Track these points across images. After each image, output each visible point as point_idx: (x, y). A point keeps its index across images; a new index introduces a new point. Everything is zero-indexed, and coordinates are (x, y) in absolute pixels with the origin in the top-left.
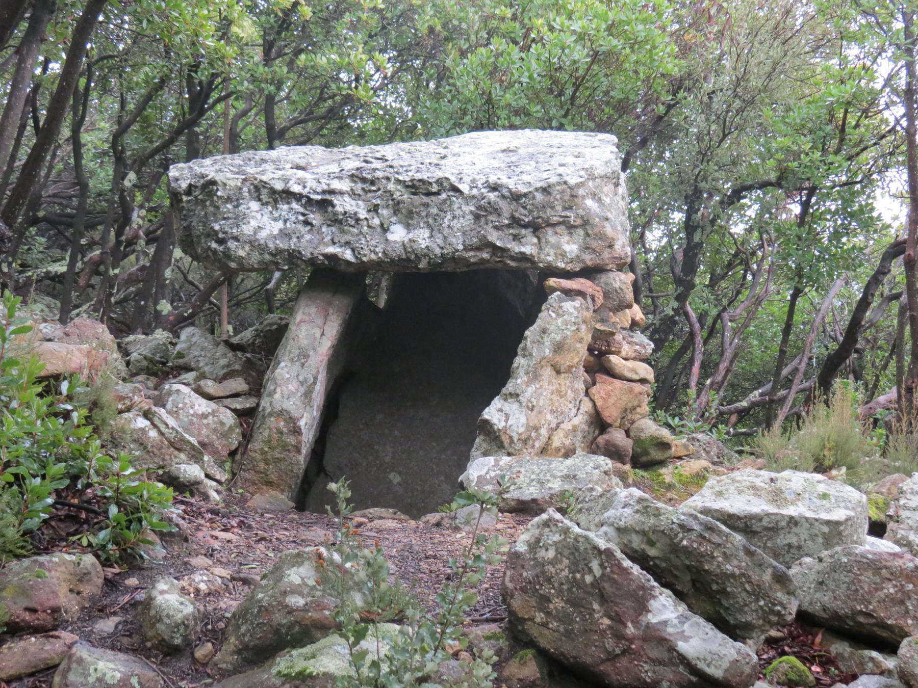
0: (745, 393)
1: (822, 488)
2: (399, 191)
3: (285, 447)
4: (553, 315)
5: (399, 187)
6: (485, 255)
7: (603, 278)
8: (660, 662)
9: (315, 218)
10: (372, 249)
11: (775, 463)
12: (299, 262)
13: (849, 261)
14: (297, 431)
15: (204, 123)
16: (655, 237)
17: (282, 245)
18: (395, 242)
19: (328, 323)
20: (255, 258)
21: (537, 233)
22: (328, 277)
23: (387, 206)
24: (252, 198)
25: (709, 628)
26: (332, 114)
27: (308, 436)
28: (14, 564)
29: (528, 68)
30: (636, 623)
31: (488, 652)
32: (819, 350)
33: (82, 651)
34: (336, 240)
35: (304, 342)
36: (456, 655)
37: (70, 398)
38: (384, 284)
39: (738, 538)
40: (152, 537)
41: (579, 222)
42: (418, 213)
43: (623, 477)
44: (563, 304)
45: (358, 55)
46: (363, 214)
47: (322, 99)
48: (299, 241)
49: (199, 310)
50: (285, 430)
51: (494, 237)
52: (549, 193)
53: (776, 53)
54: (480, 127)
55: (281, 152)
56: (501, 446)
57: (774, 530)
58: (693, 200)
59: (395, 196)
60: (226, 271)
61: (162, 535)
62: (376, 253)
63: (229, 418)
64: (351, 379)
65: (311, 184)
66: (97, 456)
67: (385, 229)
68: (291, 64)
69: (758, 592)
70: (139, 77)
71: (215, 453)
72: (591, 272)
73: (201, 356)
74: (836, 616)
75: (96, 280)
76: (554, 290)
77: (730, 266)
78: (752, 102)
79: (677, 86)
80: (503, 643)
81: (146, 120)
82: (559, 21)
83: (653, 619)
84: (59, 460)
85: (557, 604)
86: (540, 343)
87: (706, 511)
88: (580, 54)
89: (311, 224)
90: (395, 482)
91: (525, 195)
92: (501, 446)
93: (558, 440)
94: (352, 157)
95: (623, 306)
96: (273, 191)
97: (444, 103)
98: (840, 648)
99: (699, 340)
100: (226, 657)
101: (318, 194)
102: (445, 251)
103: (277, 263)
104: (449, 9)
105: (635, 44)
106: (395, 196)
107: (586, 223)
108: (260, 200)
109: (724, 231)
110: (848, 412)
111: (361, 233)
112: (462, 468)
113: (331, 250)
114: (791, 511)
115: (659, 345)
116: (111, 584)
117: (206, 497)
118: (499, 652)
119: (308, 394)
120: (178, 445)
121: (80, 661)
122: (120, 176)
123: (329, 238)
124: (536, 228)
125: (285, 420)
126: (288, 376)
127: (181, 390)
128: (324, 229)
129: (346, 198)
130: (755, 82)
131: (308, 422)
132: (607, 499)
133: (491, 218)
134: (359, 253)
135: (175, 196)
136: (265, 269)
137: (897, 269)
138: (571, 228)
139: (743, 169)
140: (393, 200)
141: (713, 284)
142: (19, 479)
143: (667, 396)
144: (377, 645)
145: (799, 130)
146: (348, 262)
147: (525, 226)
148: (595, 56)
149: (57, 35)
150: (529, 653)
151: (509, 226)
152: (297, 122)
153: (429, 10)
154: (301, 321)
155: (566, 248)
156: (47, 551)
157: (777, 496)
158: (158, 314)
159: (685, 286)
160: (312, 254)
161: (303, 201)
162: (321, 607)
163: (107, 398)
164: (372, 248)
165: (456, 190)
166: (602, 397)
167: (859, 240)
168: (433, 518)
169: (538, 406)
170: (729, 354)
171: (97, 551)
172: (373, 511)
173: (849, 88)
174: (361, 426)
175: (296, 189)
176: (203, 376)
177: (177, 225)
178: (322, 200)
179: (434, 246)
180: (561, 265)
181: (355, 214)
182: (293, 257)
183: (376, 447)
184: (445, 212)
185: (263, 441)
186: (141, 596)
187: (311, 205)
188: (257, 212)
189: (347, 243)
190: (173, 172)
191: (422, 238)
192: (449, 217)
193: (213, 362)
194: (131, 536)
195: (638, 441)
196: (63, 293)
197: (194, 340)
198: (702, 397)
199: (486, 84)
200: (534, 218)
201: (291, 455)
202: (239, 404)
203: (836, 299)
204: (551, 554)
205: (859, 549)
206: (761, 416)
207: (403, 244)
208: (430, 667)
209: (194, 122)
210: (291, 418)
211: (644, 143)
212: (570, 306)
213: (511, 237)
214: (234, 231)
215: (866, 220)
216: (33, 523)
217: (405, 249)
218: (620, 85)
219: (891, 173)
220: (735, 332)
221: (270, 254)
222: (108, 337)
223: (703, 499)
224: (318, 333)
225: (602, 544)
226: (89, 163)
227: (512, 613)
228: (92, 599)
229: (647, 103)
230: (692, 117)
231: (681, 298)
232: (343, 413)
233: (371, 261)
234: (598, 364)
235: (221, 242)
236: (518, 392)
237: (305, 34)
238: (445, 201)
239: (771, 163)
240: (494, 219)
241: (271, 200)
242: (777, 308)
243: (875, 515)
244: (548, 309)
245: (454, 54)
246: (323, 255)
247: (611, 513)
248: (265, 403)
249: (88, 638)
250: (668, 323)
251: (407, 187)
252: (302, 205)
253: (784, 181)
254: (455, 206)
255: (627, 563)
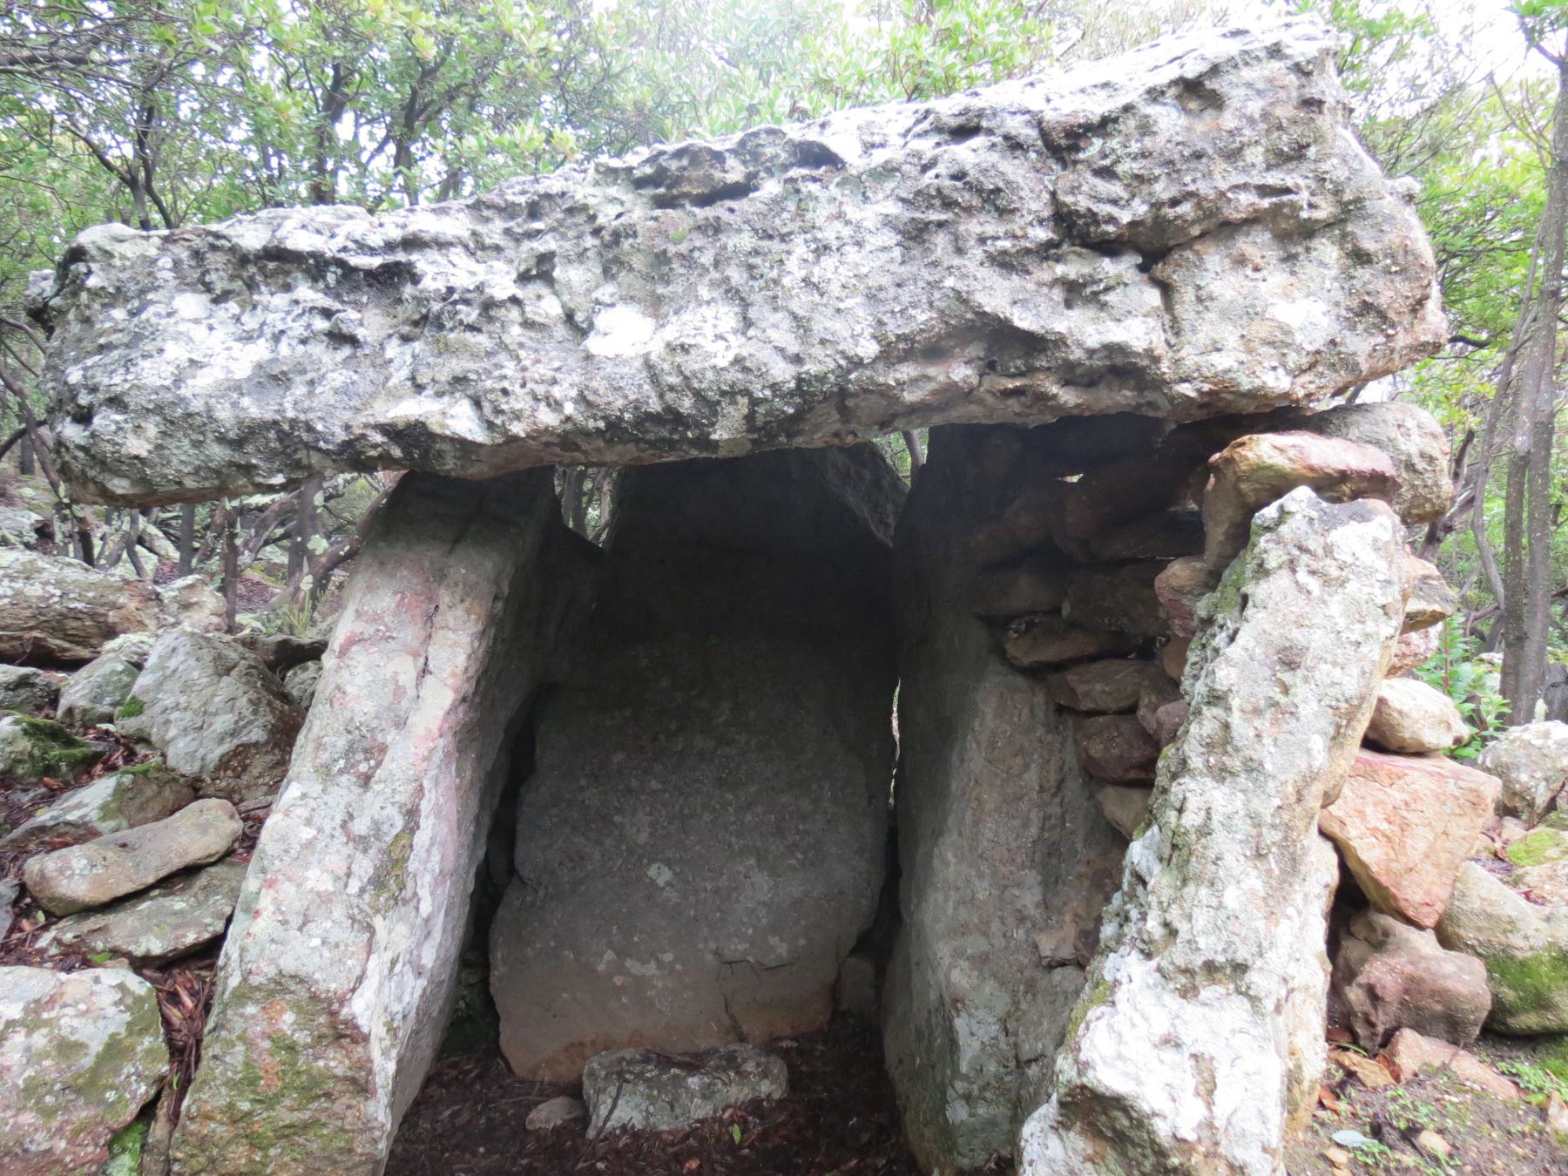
2: (613, 200)
3: (313, 1089)
4: (1314, 584)
5: (613, 191)
6: (961, 372)
9: (368, 321)
12: (315, 459)
14: (346, 1034)
17: (254, 409)
18: (617, 360)
19: (440, 635)
21: (1159, 269)
22: (438, 500)
23: (582, 256)
24: (184, 284)
34: (422, 380)
38: (606, 487)
41: (1325, 211)
42: (687, 259)
44: (1335, 536)
46: (502, 284)
48: (311, 393)
50: (302, 1037)
51: (997, 295)
52: (1215, 101)
59: (601, 220)
62: (555, 405)
73: (177, 707)
76: (1278, 484)
86: (1280, 710)
89: (352, 341)
90: (661, 882)
91: (1104, 126)
101: (373, 251)
102: (811, 368)
103: (248, 469)
104: (661, 78)
106: (601, 220)
108: (208, 288)
111: (503, 346)
113: (408, 409)
119: (389, 879)
123: (405, 373)
124: (1155, 248)
125: (297, 1008)
126: (307, 833)
128: (393, 349)
129: (457, 254)
133: (972, 227)
134: (498, 411)
140: (597, 232)
146: (464, 446)
147: (1109, 248)
151: (1046, 252)
154: (351, 642)
160: (347, 427)
161: (331, 279)
164: (541, 390)
165: (818, 157)
166: (1375, 832)
174: (583, 782)
178: (385, 267)
179: (765, 355)
180: (1278, 382)
181: (480, 288)
182: (293, 450)
183: (617, 819)
184: (784, 238)
185: (231, 1084)
187: (356, 288)
188: (197, 321)
189: (459, 381)
192: (800, 248)
197: (172, 664)
200: (1156, 206)
201: (338, 1107)
207: (648, 365)
210: (314, 998)
213: (1058, 294)
214: (117, 379)
217: (655, 379)
221: (222, 439)
224: (407, 670)
232: (546, 758)
233: (538, 434)
235: (84, 417)
236: (1242, 955)
238: (777, 203)
240: (990, 229)
241: (238, 285)
244: (1292, 565)
246: (385, 429)
251: (640, 183)
252: (327, 290)
254: (820, 214)
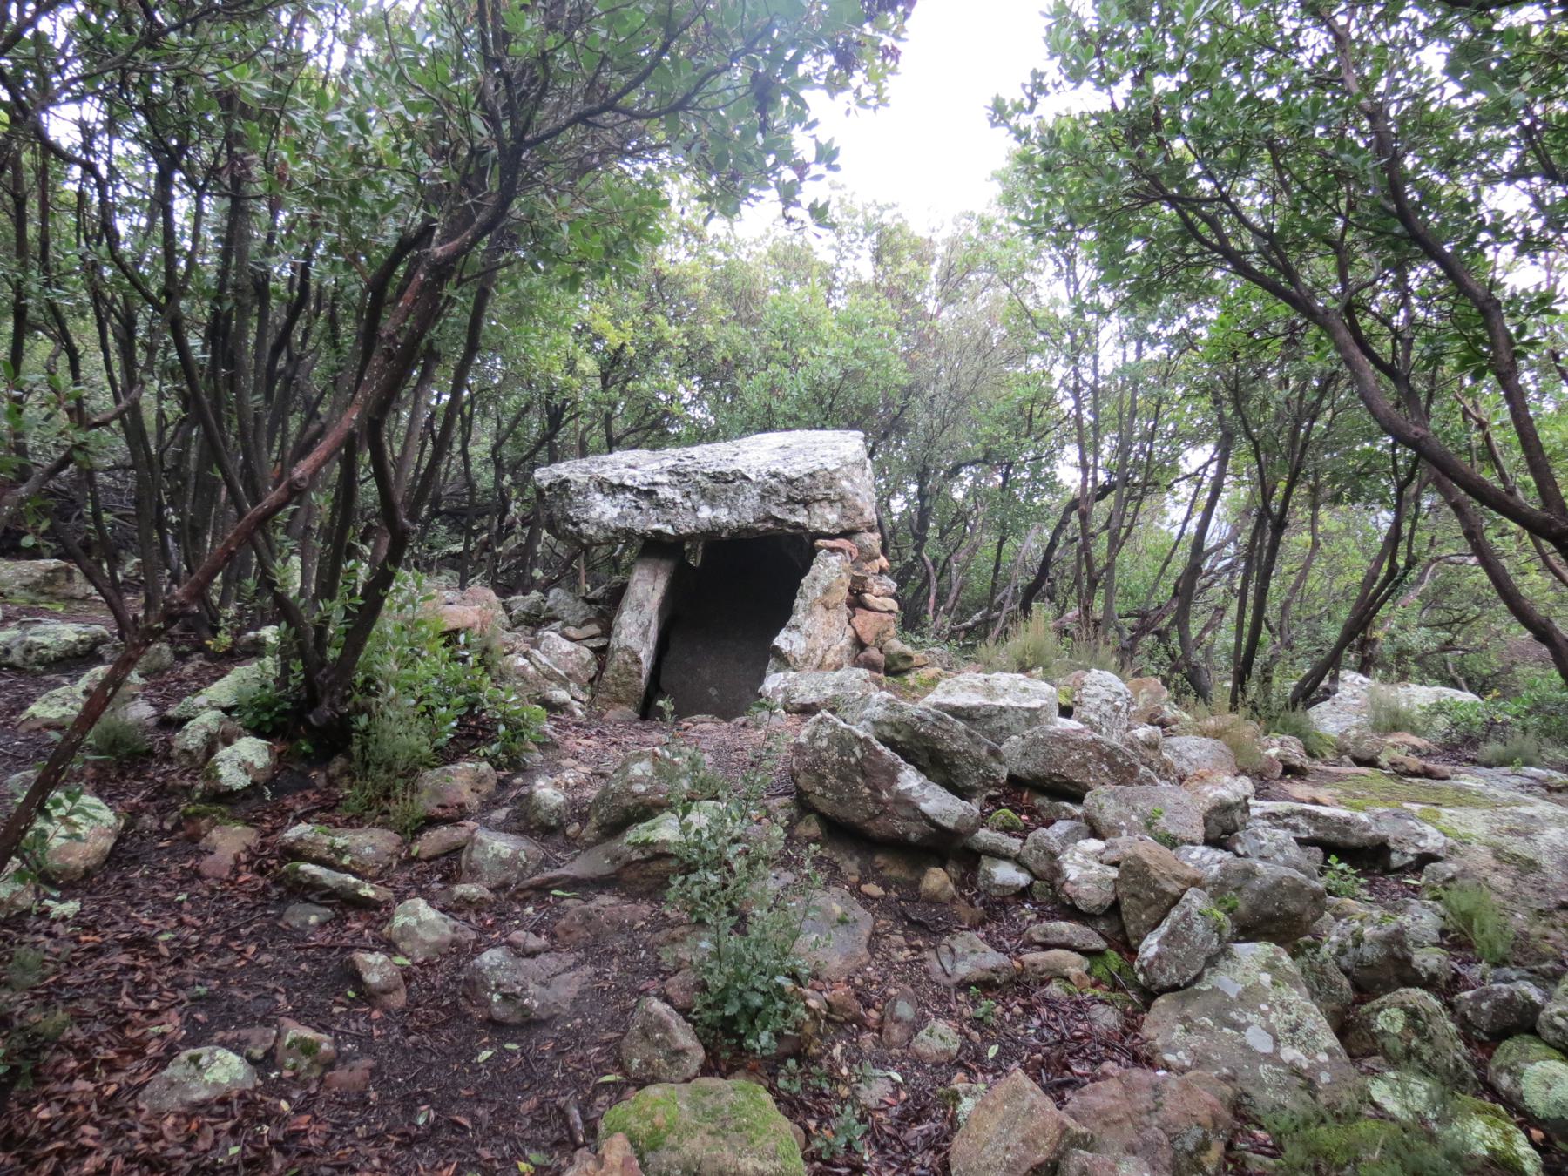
0: (970, 615)
1: (1023, 684)
3: (630, 673)
7: (857, 538)
8: (908, 819)
9: (644, 504)
10: (687, 525)
11: (989, 667)
13: (1040, 515)
14: (638, 661)
15: (561, 436)
16: (898, 505)
17: (621, 525)
20: (601, 535)
22: (655, 547)
25: (942, 792)
26: (654, 425)
27: (646, 664)
28: (429, 773)
29: (795, 385)
30: (889, 791)
31: (781, 818)
32: (1022, 580)
33: (482, 835)
35: (640, 595)
36: (759, 822)
37: (467, 646)
39: (961, 725)
40: (532, 746)
43: (879, 683)
45: (671, 379)
46: (679, 499)
47: (647, 414)
49: (563, 575)
51: (776, 512)
53: (978, 364)
54: (764, 430)
55: (618, 455)
56: (788, 665)
57: (989, 717)
58: (922, 478)
60: (581, 546)
61: (539, 745)
63: (587, 655)
64: (676, 622)
65: (640, 479)
66: (487, 688)
67: (695, 510)
68: (622, 390)
69: (978, 764)
70: (510, 404)
71: (578, 680)
72: (847, 534)
74: (1037, 778)
75: (486, 555)
77: (954, 522)
78: (962, 402)
79: (907, 392)
80: (793, 810)
81: (517, 436)
82: (818, 349)
83: (901, 787)
84: (459, 693)
85: (831, 780)
87: (938, 706)
88: (835, 373)
92: (788, 665)
93: (830, 658)
94: (670, 457)
95: (872, 558)
96: (612, 486)
97: (737, 415)
98: (1041, 801)
99: (933, 578)
100: (590, 833)
105: (875, 364)
107: (842, 498)
109: (948, 497)
110: (1042, 627)
112: (761, 682)
113: (656, 527)
114: (1001, 702)
115: (902, 583)
116: (503, 784)
117: (572, 714)
118: (790, 818)
119: (645, 634)
120: (550, 676)
121: (481, 843)
122: (499, 477)
124: (806, 503)
127: (550, 635)
130: (964, 387)
131: (646, 653)
132: (865, 701)
135: (540, 492)
136: (611, 542)
137: (1075, 518)
138: (831, 502)
139: (959, 451)
141: (943, 534)
142: (430, 709)
143: (911, 620)
144: (699, 818)
145: (999, 420)
148: (846, 373)
149: (444, 375)
150: (812, 817)
152: (629, 432)
153: (722, 345)
155: (827, 517)
156: (453, 762)
157: (990, 691)
158: (533, 579)
159: (920, 539)
162: (657, 791)
163: (495, 644)
167: (1047, 498)
168: (740, 720)
169: (814, 632)
170: (955, 587)
171: (491, 759)
172: (697, 717)
173: (1033, 389)
175: (629, 483)
176: (567, 624)
177: (543, 514)
182: (629, 533)
186: (524, 791)
190: (537, 474)
191: (723, 515)
193: (574, 613)
194: (516, 747)
195: (888, 656)
196: (463, 568)
198: (937, 620)
199: (766, 398)
202: (594, 644)
203: (1032, 543)
204: (825, 743)
205: (1052, 728)
206: (979, 632)
208: (737, 832)
209: (553, 436)
211: (885, 436)
212: (834, 560)
215: (1053, 486)
216: (442, 741)
218: (864, 395)
219: (1067, 448)
220: (960, 570)
222: (494, 598)
223: (938, 696)
225: (862, 734)
226: (475, 468)
227: (798, 788)
228: (489, 795)
229: (887, 406)
230: (921, 417)
231: (918, 548)
234: (857, 601)
235: (575, 524)
237: (631, 368)
239: (978, 446)
242: (991, 552)
243: (1064, 701)
245: (742, 376)
247: (867, 711)
248: (613, 642)
249: (486, 824)
250: (909, 568)
253: (987, 459)
255: (880, 747)
